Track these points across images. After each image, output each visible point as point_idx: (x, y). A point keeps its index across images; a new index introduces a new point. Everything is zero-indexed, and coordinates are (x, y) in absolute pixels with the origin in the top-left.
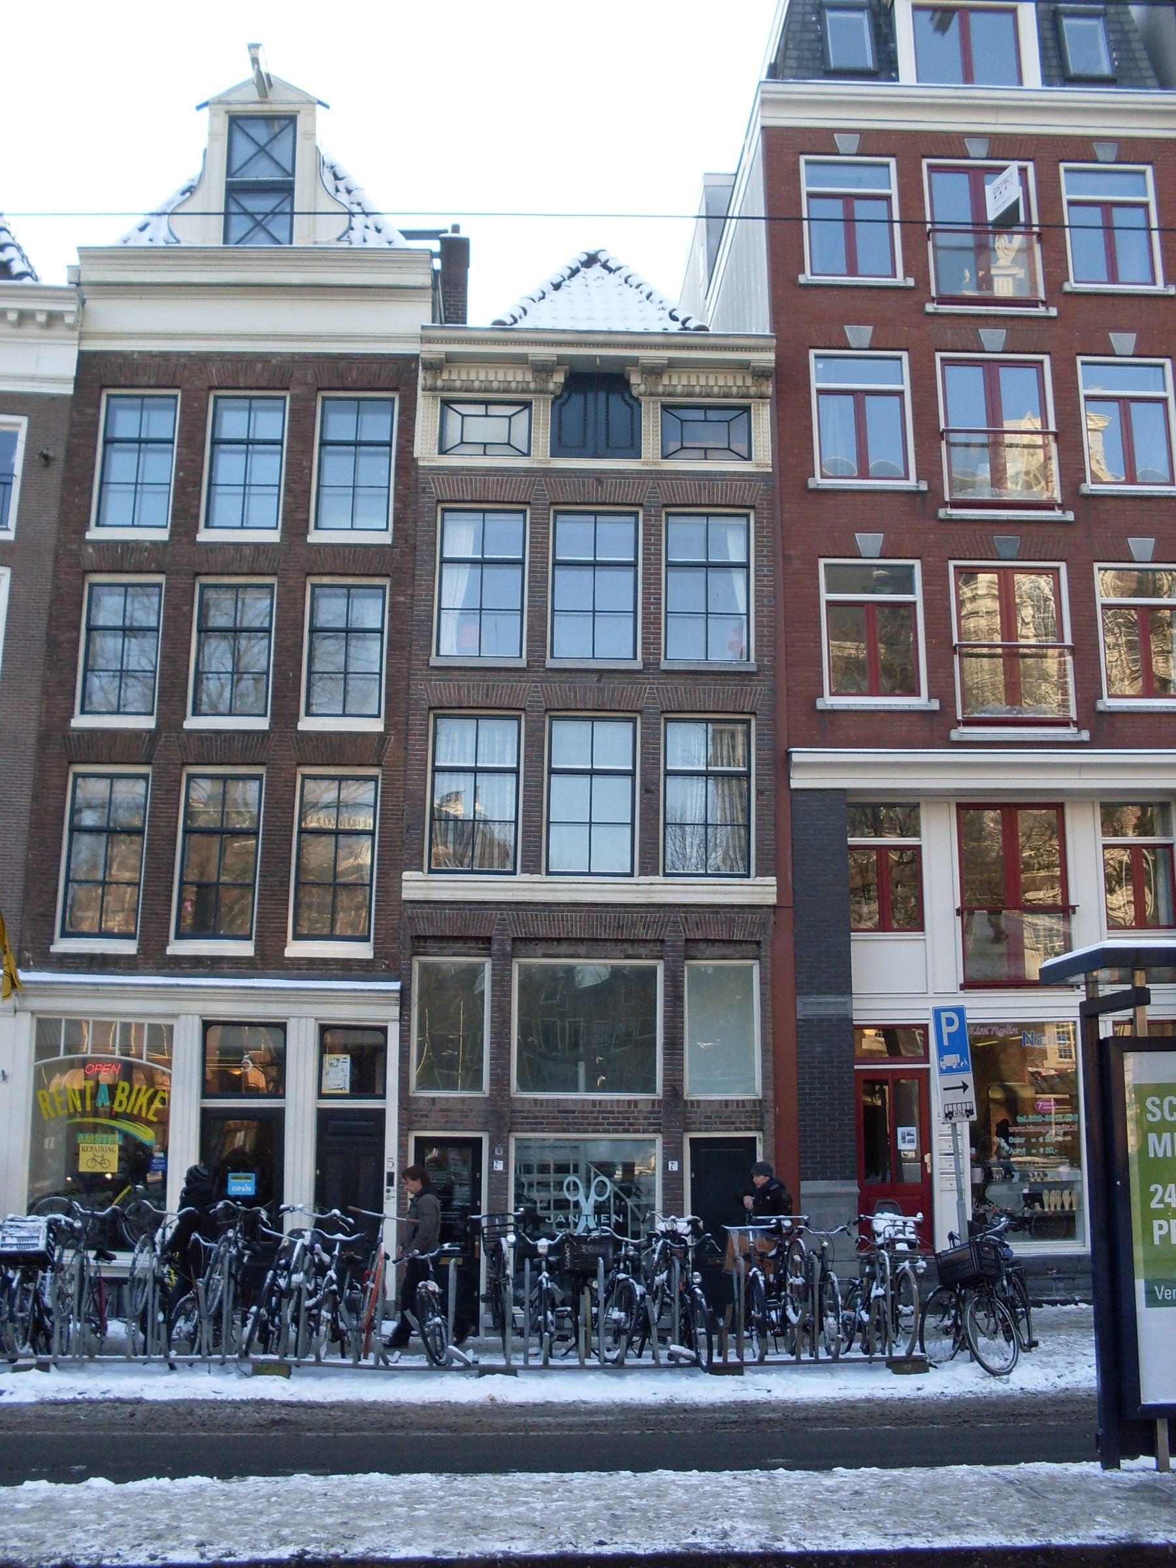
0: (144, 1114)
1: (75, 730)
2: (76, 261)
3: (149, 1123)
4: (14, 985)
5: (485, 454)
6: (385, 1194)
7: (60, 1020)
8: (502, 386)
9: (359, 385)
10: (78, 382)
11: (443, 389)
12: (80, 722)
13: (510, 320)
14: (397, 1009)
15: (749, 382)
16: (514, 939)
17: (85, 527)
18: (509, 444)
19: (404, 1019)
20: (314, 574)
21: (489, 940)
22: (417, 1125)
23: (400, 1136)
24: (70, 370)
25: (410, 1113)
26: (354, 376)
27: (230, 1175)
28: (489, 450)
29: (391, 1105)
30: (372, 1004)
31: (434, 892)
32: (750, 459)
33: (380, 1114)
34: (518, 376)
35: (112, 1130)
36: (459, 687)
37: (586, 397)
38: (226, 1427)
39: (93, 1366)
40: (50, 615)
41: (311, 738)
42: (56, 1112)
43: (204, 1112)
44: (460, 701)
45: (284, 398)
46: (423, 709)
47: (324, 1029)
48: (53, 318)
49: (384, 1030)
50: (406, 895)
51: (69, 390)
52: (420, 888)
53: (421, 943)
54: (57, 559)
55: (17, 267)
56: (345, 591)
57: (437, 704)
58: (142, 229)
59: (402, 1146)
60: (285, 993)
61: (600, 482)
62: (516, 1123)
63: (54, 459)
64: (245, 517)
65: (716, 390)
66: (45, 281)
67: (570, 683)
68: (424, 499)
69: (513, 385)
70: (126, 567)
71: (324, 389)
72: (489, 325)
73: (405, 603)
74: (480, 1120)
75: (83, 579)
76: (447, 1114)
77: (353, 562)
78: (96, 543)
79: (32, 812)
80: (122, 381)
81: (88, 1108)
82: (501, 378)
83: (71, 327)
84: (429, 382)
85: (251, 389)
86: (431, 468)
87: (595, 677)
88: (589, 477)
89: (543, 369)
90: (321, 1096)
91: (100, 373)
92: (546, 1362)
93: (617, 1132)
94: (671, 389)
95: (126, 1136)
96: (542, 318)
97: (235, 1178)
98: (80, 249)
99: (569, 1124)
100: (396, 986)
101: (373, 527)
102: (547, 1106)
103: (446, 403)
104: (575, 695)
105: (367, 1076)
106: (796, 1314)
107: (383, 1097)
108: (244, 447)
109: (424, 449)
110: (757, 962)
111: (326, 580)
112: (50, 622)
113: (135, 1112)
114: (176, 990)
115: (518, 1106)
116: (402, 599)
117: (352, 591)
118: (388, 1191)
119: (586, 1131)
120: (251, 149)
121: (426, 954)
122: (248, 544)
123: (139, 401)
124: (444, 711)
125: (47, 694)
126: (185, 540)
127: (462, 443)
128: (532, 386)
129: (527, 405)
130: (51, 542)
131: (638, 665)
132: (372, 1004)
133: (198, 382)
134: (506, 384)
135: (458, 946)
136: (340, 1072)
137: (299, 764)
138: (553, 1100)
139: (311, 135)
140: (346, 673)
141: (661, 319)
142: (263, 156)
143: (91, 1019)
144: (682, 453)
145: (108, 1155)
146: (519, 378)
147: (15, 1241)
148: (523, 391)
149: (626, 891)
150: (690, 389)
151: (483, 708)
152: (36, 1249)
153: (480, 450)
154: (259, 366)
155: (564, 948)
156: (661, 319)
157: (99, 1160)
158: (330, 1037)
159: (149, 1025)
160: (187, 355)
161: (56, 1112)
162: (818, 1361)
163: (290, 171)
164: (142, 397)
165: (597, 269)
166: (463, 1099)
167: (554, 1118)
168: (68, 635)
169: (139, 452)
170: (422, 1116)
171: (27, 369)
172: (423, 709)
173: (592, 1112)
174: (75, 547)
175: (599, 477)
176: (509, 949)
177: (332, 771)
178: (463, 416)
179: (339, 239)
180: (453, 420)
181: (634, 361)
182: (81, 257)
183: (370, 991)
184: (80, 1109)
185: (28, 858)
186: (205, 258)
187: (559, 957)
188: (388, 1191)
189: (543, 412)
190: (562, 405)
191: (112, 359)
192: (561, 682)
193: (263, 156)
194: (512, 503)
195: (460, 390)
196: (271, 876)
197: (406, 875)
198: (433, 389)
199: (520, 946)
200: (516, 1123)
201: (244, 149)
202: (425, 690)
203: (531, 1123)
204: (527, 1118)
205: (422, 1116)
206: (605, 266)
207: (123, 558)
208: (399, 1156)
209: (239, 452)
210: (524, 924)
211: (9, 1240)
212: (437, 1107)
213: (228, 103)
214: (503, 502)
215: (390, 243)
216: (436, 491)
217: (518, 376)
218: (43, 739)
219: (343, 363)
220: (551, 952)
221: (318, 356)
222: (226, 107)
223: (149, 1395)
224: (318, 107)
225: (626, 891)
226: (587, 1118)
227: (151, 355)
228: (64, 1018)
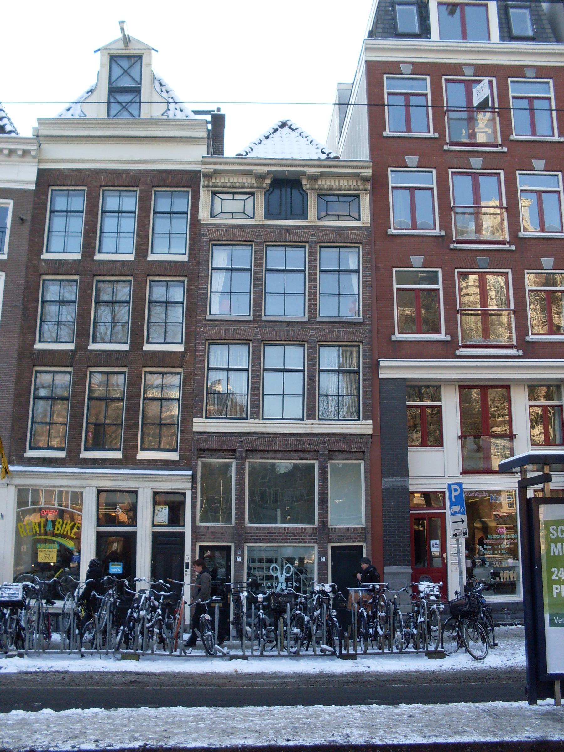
0: (69, 534)
1: (36, 350)
2: (36, 125)
3: (71, 539)
4: (7, 473)
5: (233, 218)
6: (185, 573)
7: (29, 489)
8: (241, 185)
9: (172, 185)
10: (38, 183)
11: (212, 187)
12: (38, 346)
13: (245, 154)
14: (191, 484)
15: (359, 183)
16: (247, 450)
17: (41, 253)
18: (244, 213)
19: (194, 489)
20: (151, 275)
21: (234, 451)
22: (200, 540)
23: (192, 545)
24: (34, 177)
25: (197, 534)
26: (170, 180)
27: (110, 563)
28: (235, 216)
29: (188, 530)
30: (178, 482)
31: (208, 428)
32: (360, 220)
33: (182, 534)
34: (248, 180)
35: (54, 542)
36: (220, 330)
37: (281, 190)
38: (109, 684)
39: (44, 655)
40: (24, 295)
41: (149, 354)
42: (27, 533)
43: (98, 533)
44: (221, 336)
45: (136, 191)
46: (203, 340)
47: (155, 493)
48: (26, 153)
49: (184, 494)
50: (195, 429)
51: (33, 187)
52: (201, 426)
53: (202, 452)
54: (27, 268)
55: (8, 128)
56: (165, 283)
57: (209, 338)
58: (68, 110)
59: (193, 550)
60: (136, 476)
61: (288, 231)
62: (248, 539)
63: (26, 220)
64: (118, 248)
65: (343, 187)
66: (22, 135)
67: (274, 327)
68: (204, 240)
69: (246, 185)
70: (61, 272)
71: (155, 187)
72: (234, 156)
73: (194, 289)
74: (230, 537)
75: (40, 278)
76: (214, 534)
77: (169, 270)
78: (46, 261)
79: (16, 389)
80: (59, 183)
81: (42, 531)
82: (240, 181)
83: (34, 157)
84: (206, 183)
85: (120, 186)
86: (207, 225)
87: (285, 325)
88: (283, 229)
89: (260, 177)
90: (154, 526)
91: (48, 179)
92: (262, 653)
93: (296, 543)
94: (322, 187)
95: (61, 545)
96: (260, 152)
97: (113, 565)
98: (38, 119)
99: (273, 539)
100: (190, 473)
101: (179, 253)
102: (263, 530)
103: (214, 193)
104: (276, 333)
105: (176, 516)
106: (382, 630)
107: (184, 526)
108: (117, 214)
109: (204, 215)
110: (363, 461)
111: (156, 278)
112: (24, 298)
113: (65, 533)
114: (84, 475)
115: (248, 530)
116: (193, 287)
117: (169, 283)
118: (186, 571)
119: (281, 543)
120: (120, 72)
121: (204, 458)
122: (119, 261)
123: (66, 192)
124: (213, 341)
125: (23, 333)
126: (89, 259)
127: (222, 212)
128: (255, 185)
129: (253, 194)
130: (25, 260)
131: (306, 319)
132: (178, 482)
133: (95, 183)
134: (242, 184)
135: (220, 454)
136: (163, 514)
137: (143, 367)
138: (265, 528)
139: (149, 65)
140: (166, 323)
141: (317, 153)
142: (126, 75)
143: (44, 489)
144: (327, 217)
145: (52, 554)
146: (249, 181)
147: (7, 595)
148: (251, 188)
149: (300, 428)
150: (331, 187)
151: (232, 340)
152: (17, 599)
153: (230, 216)
154: (124, 175)
155: (270, 455)
156: (317, 153)
157: (48, 556)
158: (158, 497)
159: (72, 491)
160: (90, 170)
161: (27, 533)
162: (392, 653)
163: (139, 82)
164: (68, 190)
165: (286, 129)
166: (222, 527)
167: (265, 536)
168: (33, 305)
169: (67, 217)
170: (202, 535)
171: (13, 177)
172: (203, 340)
173: (284, 533)
174: (36, 262)
175: (287, 229)
176: (244, 455)
177: (159, 370)
178: (222, 200)
179: (162, 115)
180: (217, 201)
181: (304, 173)
182: (39, 123)
183: (177, 475)
184: (38, 532)
185: (13, 412)
186: (98, 124)
187: (268, 459)
188: (186, 571)
189: (260, 198)
190: (270, 194)
191: (54, 172)
192: (269, 327)
193: (126, 75)
194: (246, 241)
195: (221, 187)
196: (130, 420)
197: (195, 420)
198: (208, 186)
199: (250, 453)
200: (248, 539)
201: (117, 71)
202: (204, 331)
203: (255, 539)
204: (253, 536)
205: (202, 535)
206: (290, 128)
207: (59, 267)
208: (191, 554)
209: (114, 217)
210: (251, 443)
211: (4, 595)
212: (210, 531)
213: (110, 49)
214: (241, 241)
215: (187, 116)
216: (209, 235)
217: (248, 180)
218: (21, 355)
219: (164, 174)
220: (264, 456)
221: (152, 171)
222: (109, 51)
223: (72, 669)
224: (153, 51)
225: (300, 428)
226: (281, 536)
227: (72, 170)
228: (30, 488)
